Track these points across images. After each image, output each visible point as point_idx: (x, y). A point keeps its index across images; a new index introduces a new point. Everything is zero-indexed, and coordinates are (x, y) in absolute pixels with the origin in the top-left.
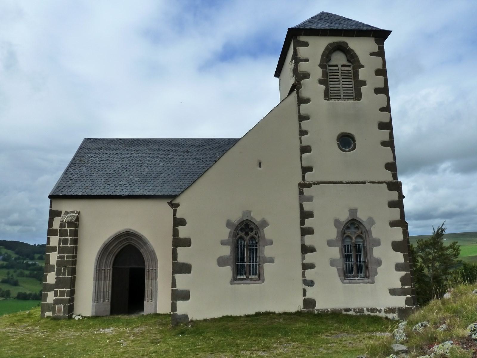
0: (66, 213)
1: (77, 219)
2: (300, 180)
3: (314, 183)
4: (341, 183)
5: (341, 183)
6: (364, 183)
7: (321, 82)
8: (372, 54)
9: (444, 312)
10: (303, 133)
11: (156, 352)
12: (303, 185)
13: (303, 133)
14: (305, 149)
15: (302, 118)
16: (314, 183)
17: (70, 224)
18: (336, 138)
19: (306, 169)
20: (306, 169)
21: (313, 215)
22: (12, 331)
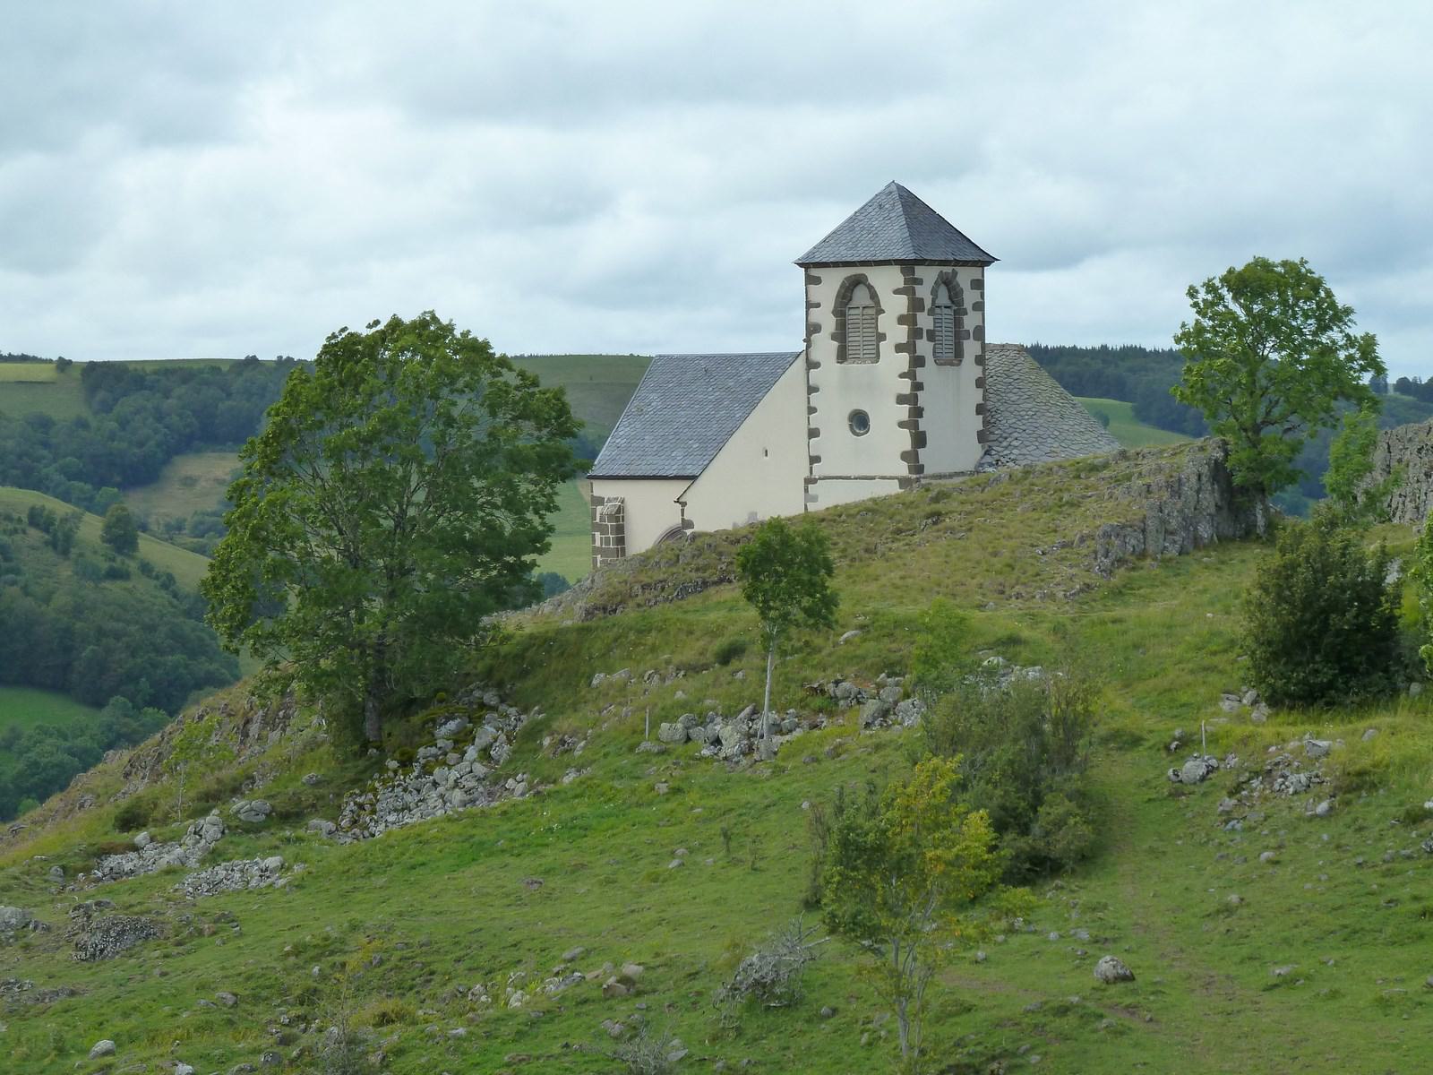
0: (609, 500)
1: (620, 510)
2: (807, 474)
3: (820, 479)
4: (848, 478)
5: (848, 478)
6: (872, 478)
7: (834, 337)
8: (818, 305)
9: (1092, 767)
10: (812, 410)
11: (1128, 978)
12: (810, 481)
13: (812, 410)
14: (813, 433)
15: (812, 389)
16: (820, 479)
17: (611, 517)
18: (847, 416)
19: (814, 460)
20: (814, 460)
21: (91, 362)
22: (1068, 931)
